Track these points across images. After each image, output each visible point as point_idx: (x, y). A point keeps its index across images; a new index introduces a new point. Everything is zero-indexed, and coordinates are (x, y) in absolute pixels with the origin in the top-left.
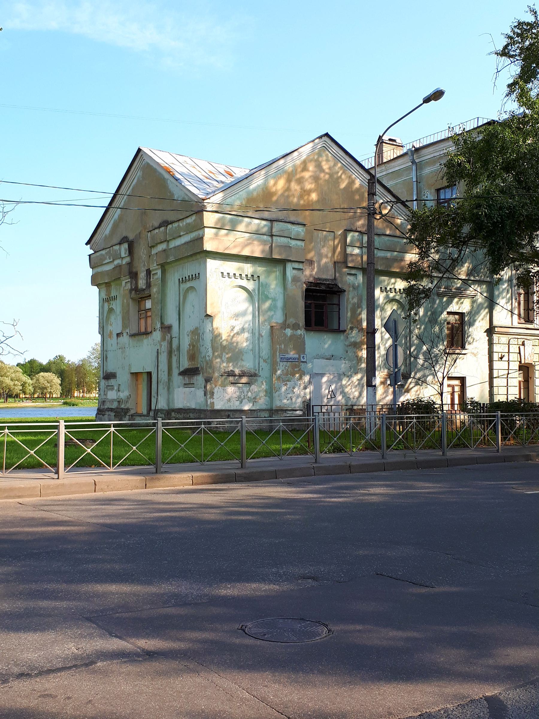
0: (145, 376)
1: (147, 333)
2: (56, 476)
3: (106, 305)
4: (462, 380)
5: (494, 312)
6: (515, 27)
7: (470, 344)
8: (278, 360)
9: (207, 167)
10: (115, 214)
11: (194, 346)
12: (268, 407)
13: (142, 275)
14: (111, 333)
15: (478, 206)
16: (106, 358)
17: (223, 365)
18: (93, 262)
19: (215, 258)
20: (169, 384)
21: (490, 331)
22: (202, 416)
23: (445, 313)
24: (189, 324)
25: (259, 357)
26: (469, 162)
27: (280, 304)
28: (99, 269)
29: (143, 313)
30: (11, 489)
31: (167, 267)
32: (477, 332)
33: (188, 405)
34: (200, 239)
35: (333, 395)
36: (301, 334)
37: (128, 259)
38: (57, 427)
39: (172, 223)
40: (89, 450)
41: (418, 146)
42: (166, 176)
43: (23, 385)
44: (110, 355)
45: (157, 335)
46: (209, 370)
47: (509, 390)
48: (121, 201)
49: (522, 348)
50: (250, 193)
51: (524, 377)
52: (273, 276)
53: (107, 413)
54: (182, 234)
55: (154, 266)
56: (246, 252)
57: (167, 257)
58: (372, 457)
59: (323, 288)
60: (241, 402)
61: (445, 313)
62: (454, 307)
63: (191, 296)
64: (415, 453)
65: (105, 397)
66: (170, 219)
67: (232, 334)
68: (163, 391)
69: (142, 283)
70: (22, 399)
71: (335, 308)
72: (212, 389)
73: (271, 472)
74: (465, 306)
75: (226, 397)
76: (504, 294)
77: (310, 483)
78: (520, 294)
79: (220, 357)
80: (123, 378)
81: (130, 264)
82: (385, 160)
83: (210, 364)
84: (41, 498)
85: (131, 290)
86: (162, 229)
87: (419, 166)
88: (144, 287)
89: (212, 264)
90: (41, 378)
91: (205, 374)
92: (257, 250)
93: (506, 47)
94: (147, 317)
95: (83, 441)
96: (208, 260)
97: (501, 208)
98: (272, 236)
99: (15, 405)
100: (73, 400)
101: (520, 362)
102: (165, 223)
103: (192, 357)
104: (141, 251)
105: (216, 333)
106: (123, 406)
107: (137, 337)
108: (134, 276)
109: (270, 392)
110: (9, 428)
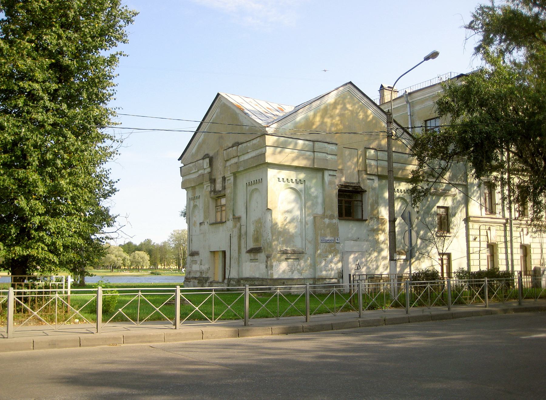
0: (221, 254)
1: (222, 223)
2: (174, 327)
3: (192, 202)
4: (449, 255)
5: (469, 207)
6: (478, 9)
7: (452, 228)
8: (320, 241)
9: (266, 105)
10: (201, 137)
11: (258, 231)
12: (313, 276)
13: (219, 181)
14: (195, 222)
15: (465, 132)
16: (192, 241)
17: (278, 246)
18: (183, 172)
19: (273, 168)
20: (239, 259)
21: (467, 220)
22: (264, 283)
23: (435, 207)
24: (254, 215)
25: (306, 239)
26: (453, 101)
27: (320, 200)
28: (187, 177)
29: (219, 208)
30: (144, 336)
31: (237, 175)
32: (458, 220)
33: (254, 275)
34: (263, 154)
35: (358, 268)
36: (335, 223)
37: (209, 170)
38: (175, 291)
39: (241, 144)
40: (197, 308)
41: (409, 91)
42: (238, 111)
43: (124, 260)
44: (194, 239)
45: (230, 224)
46: (269, 249)
47: (480, 264)
48: (205, 128)
49: (489, 231)
50: (296, 123)
51: (490, 253)
52: (314, 181)
53: (192, 280)
54: (249, 151)
55: (228, 174)
56: (295, 164)
57: (238, 167)
58: (398, 313)
59: (351, 189)
60: (293, 273)
61: (435, 207)
62: (441, 203)
63: (256, 196)
64: (429, 309)
65: (190, 269)
66: (240, 141)
67: (285, 223)
68: (234, 265)
69: (219, 187)
70: (123, 270)
71: (359, 204)
72: (271, 263)
73: (329, 325)
74: (448, 202)
75: (282, 268)
76: (475, 194)
77: (362, 333)
78: (485, 194)
79: (277, 239)
80: (205, 255)
81: (210, 173)
82: (386, 101)
83: (270, 245)
84: (165, 343)
85: (211, 192)
86: (235, 148)
87: (411, 105)
88: (220, 189)
89: (272, 173)
90: (136, 255)
91: (266, 252)
92: (302, 163)
93: (472, 22)
94: (222, 211)
95: (154, 302)
96: (269, 169)
97: (481, 133)
98: (314, 152)
99: (118, 274)
100: (158, 271)
101: (488, 242)
102: (237, 144)
103: (256, 240)
104: (219, 164)
105: (274, 222)
106: (204, 276)
107: (214, 226)
108: (213, 181)
109: (314, 266)
110: (142, 291)
